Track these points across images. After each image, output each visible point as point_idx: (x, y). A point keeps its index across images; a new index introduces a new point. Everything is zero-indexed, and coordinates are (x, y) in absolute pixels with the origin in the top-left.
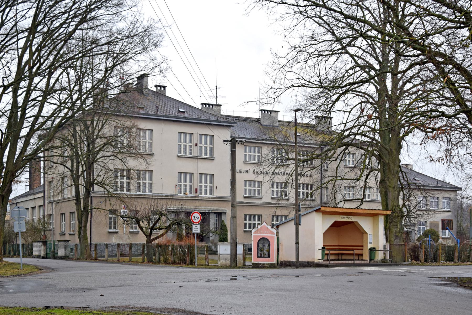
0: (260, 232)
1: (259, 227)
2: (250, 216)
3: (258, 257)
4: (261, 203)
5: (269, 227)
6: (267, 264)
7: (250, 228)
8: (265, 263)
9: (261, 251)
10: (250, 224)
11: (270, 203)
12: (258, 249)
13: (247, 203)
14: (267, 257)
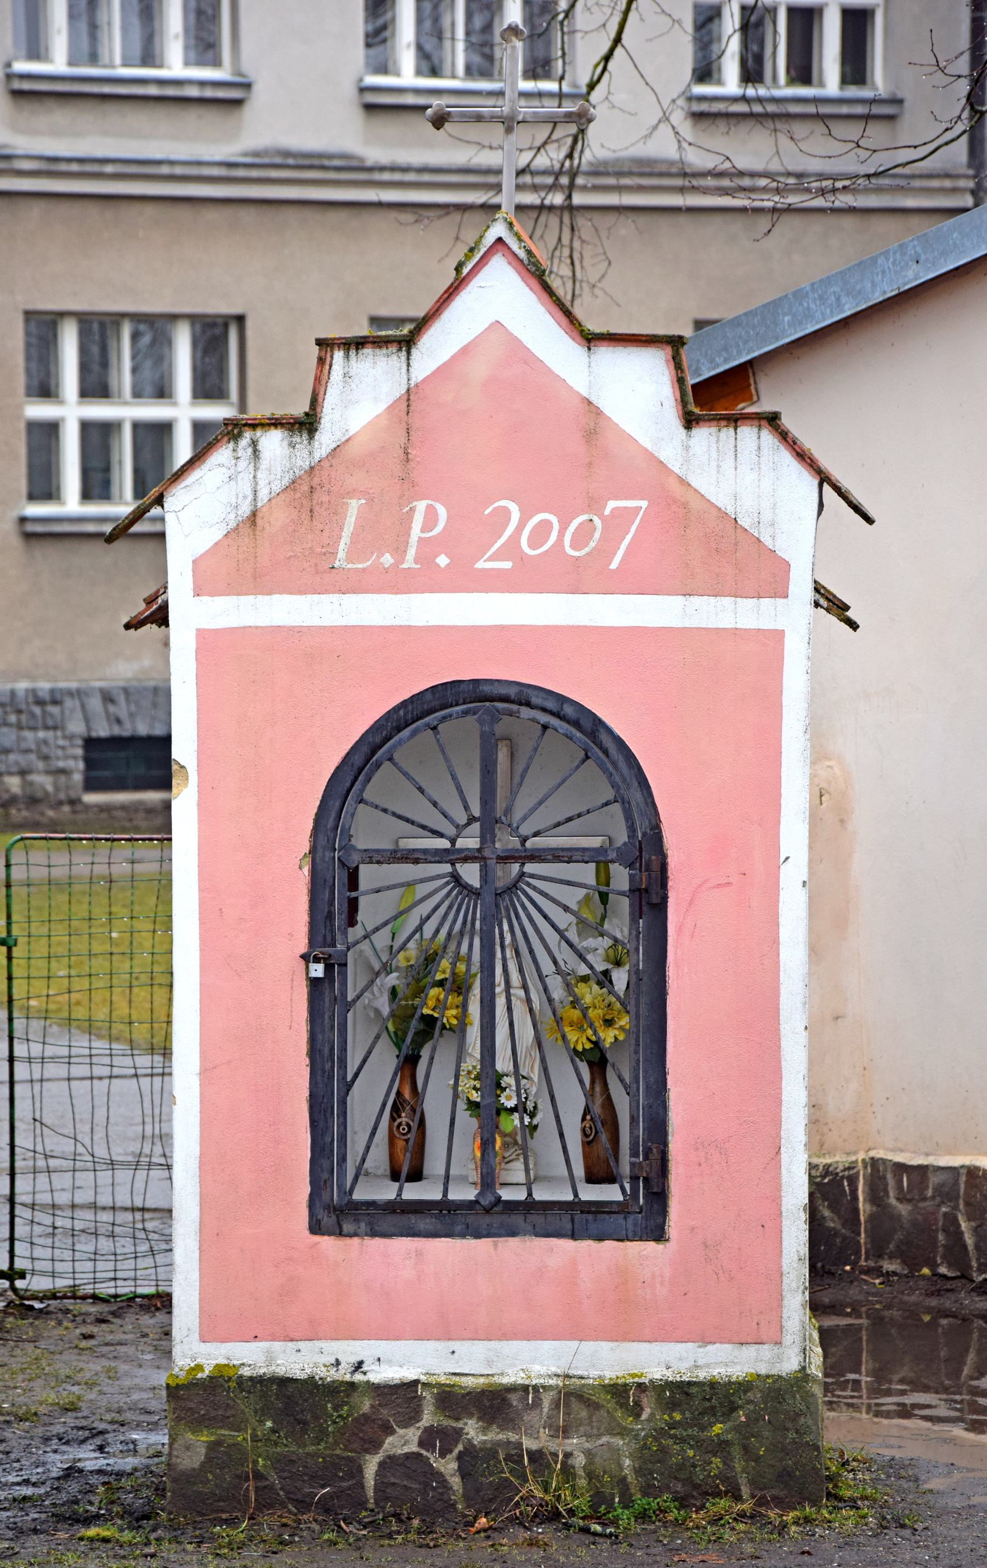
0: (387, 529)
1: (362, 396)
2: (98, 330)
3: (335, 1212)
4: (231, 170)
5: (635, 393)
6: (575, 1398)
7: (96, 484)
8: (531, 1361)
9: (415, 1034)
10: (97, 436)
11: (352, 168)
12: (326, 999)
13: (52, 166)
14: (579, 1220)
